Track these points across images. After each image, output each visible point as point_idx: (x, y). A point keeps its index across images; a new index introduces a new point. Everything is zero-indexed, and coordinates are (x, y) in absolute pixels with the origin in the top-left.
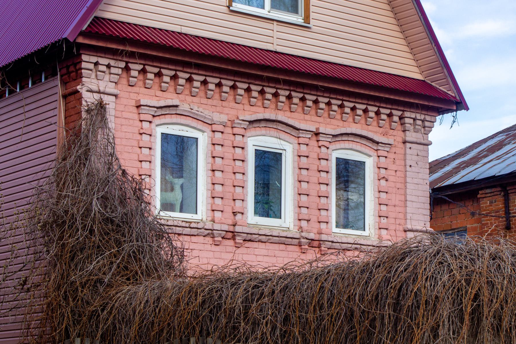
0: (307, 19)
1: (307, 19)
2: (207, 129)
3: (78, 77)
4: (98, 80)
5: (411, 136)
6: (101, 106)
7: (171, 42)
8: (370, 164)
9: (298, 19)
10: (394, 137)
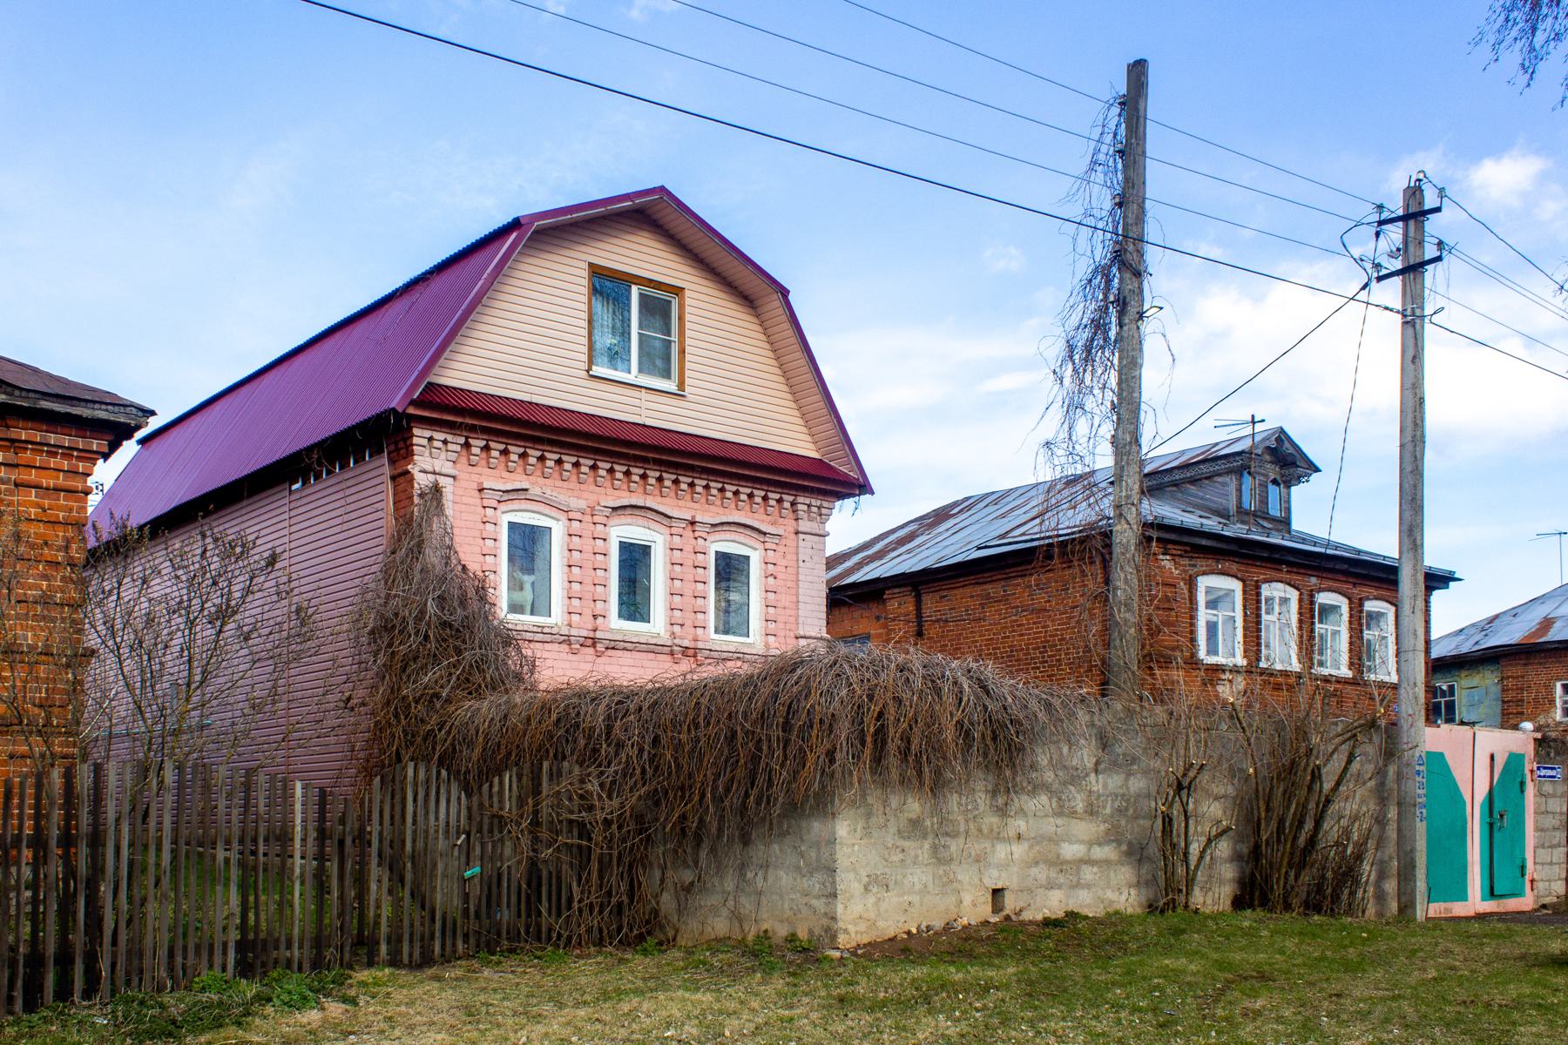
0: (681, 385)
1: (681, 385)
2: (563, 516)
3: (409, 454)
4: (434, 458)
5: (804, 525)
6: (437, 490)
7: (594, 430)
8: (558, 530)
9: (671, 386)
10: (785, 527)
